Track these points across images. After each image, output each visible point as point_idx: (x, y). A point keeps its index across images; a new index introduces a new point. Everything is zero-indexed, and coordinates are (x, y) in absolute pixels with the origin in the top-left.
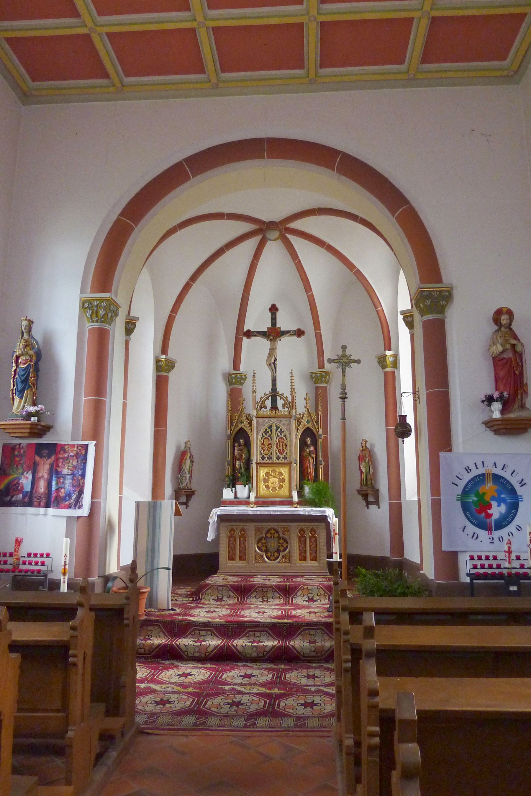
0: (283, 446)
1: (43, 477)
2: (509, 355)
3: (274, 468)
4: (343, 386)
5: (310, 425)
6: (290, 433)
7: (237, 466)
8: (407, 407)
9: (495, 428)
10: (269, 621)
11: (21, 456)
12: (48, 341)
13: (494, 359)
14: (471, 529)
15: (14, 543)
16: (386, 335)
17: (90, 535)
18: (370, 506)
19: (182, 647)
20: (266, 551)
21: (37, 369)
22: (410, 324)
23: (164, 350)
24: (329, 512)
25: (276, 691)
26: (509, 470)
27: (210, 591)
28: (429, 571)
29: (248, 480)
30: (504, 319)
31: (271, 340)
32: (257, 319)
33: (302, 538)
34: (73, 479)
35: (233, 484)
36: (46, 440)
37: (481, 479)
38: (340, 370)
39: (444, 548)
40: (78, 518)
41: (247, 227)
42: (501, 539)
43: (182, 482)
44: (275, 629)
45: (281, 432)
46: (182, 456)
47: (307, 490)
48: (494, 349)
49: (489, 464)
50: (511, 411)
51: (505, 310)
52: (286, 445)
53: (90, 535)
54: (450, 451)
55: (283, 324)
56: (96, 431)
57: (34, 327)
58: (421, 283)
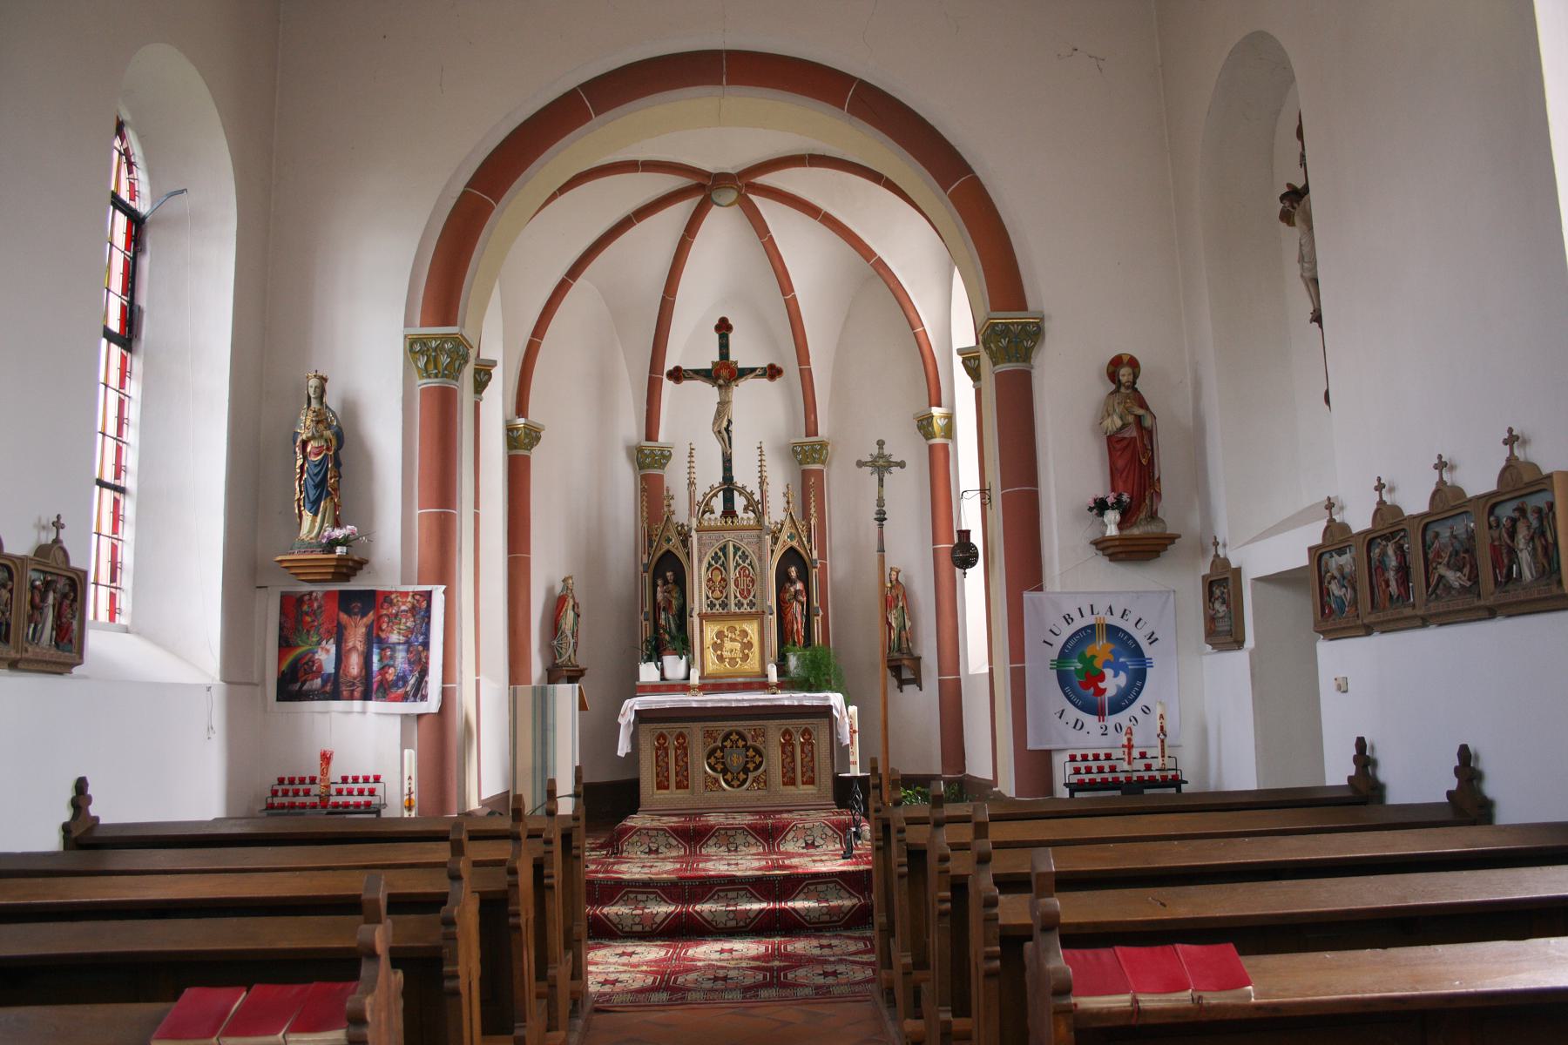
0: (750, 581)
1: (354, 647)
2: (1132, 432)
3: (732, 623)
4: (881, 502)
5: (795, 544)
6: (760, 559)
7: (663, 622)
8: (970, 516)
9: (1110, 551)
10: (749, 873)
11: (313, 613)
12: (351, 409)
13: (1110, 439)
14: (1073, 713)
15: (318, 760)
16: (931, 375)
17: (441, 742)
18: (905, 687)
19: (612, 917)
20: (725, 771)
21: (338, 464)
22: (974, 373)
23: (521, 408)
24: (836, 699)
25: (776, 963)
26: (1132, 618)
27: (635, 838)
28: (1007, 786)
29: (683, 645)
30: (1125, 373)
31: (720, 387)
32: (691, 345)
33: (788, 746)
34: (408, 651)
35: (656, 653)
36: (356, 584)
37: (1088, 633)
38: (876, 476)
39: (1029, 747)
40: (419, 716)
41: (672, 182)
42: (1118, 728)
43: (551, 650)
44: (759, 886)
45: (744, 557)
46: (557, 605)
47: (793, 661)
48: (1108, 422)
49: (1101, 609)
50: (1133, 525)
51: (1126, 359)
52: (753, 581)
53: (441, 742)
54: (1040, 589)
55: (741, 355)
56: (443, 570)
57: (328, 386)
58: (993, 309)
